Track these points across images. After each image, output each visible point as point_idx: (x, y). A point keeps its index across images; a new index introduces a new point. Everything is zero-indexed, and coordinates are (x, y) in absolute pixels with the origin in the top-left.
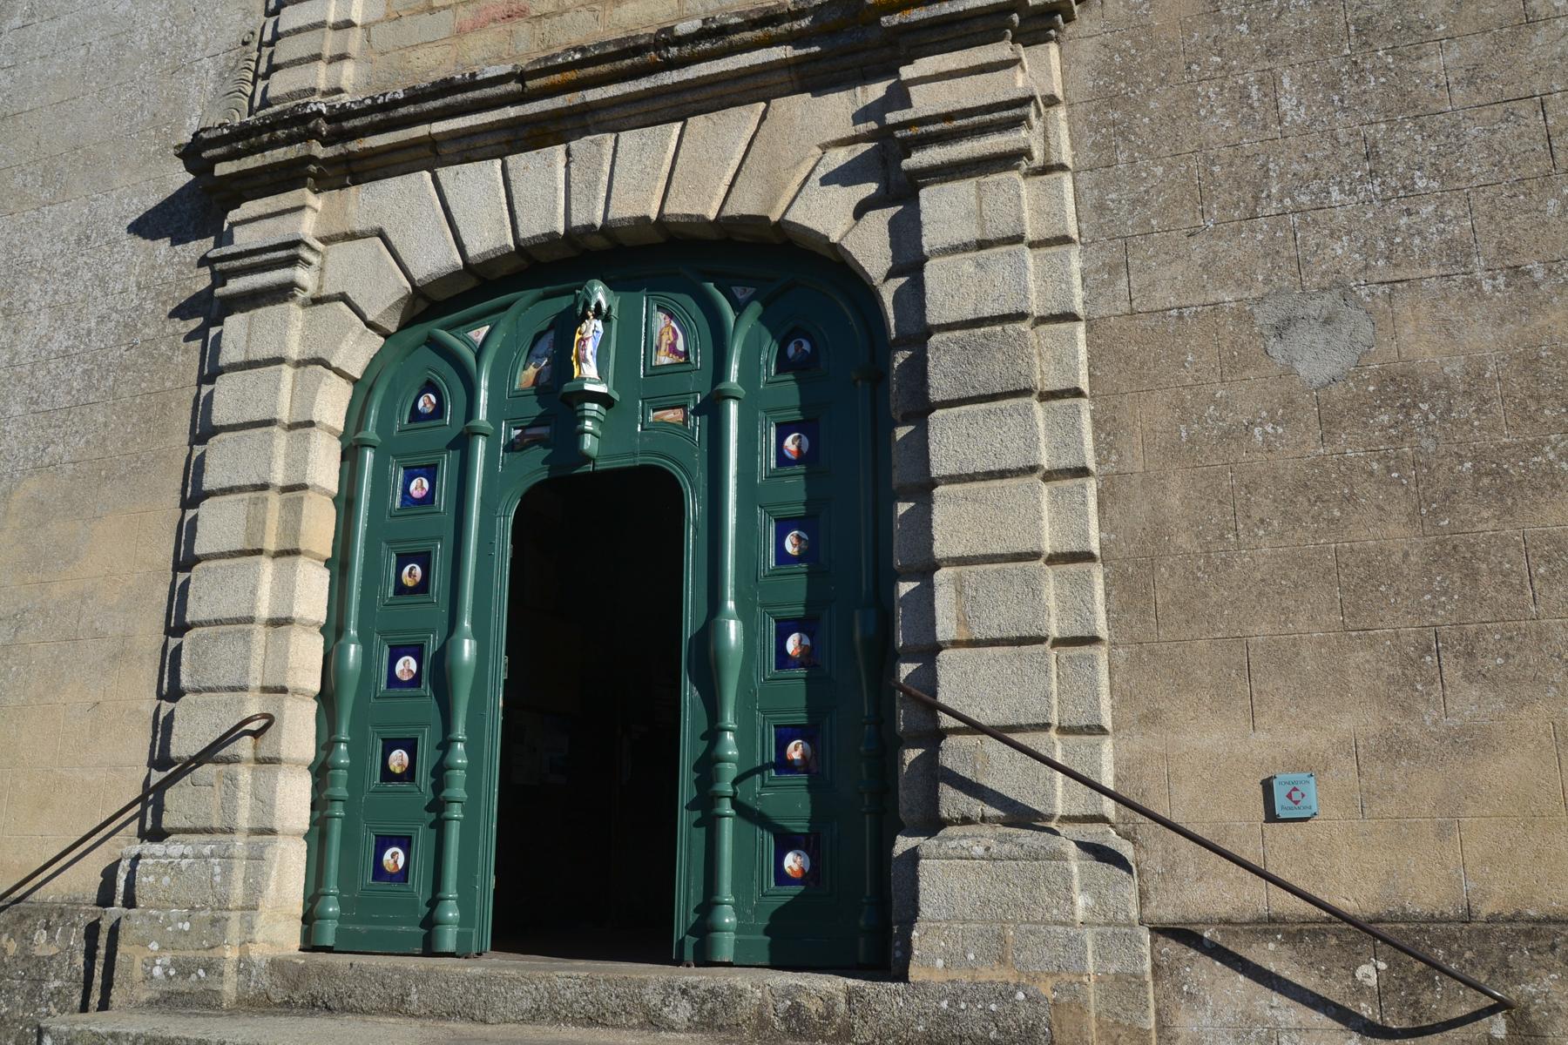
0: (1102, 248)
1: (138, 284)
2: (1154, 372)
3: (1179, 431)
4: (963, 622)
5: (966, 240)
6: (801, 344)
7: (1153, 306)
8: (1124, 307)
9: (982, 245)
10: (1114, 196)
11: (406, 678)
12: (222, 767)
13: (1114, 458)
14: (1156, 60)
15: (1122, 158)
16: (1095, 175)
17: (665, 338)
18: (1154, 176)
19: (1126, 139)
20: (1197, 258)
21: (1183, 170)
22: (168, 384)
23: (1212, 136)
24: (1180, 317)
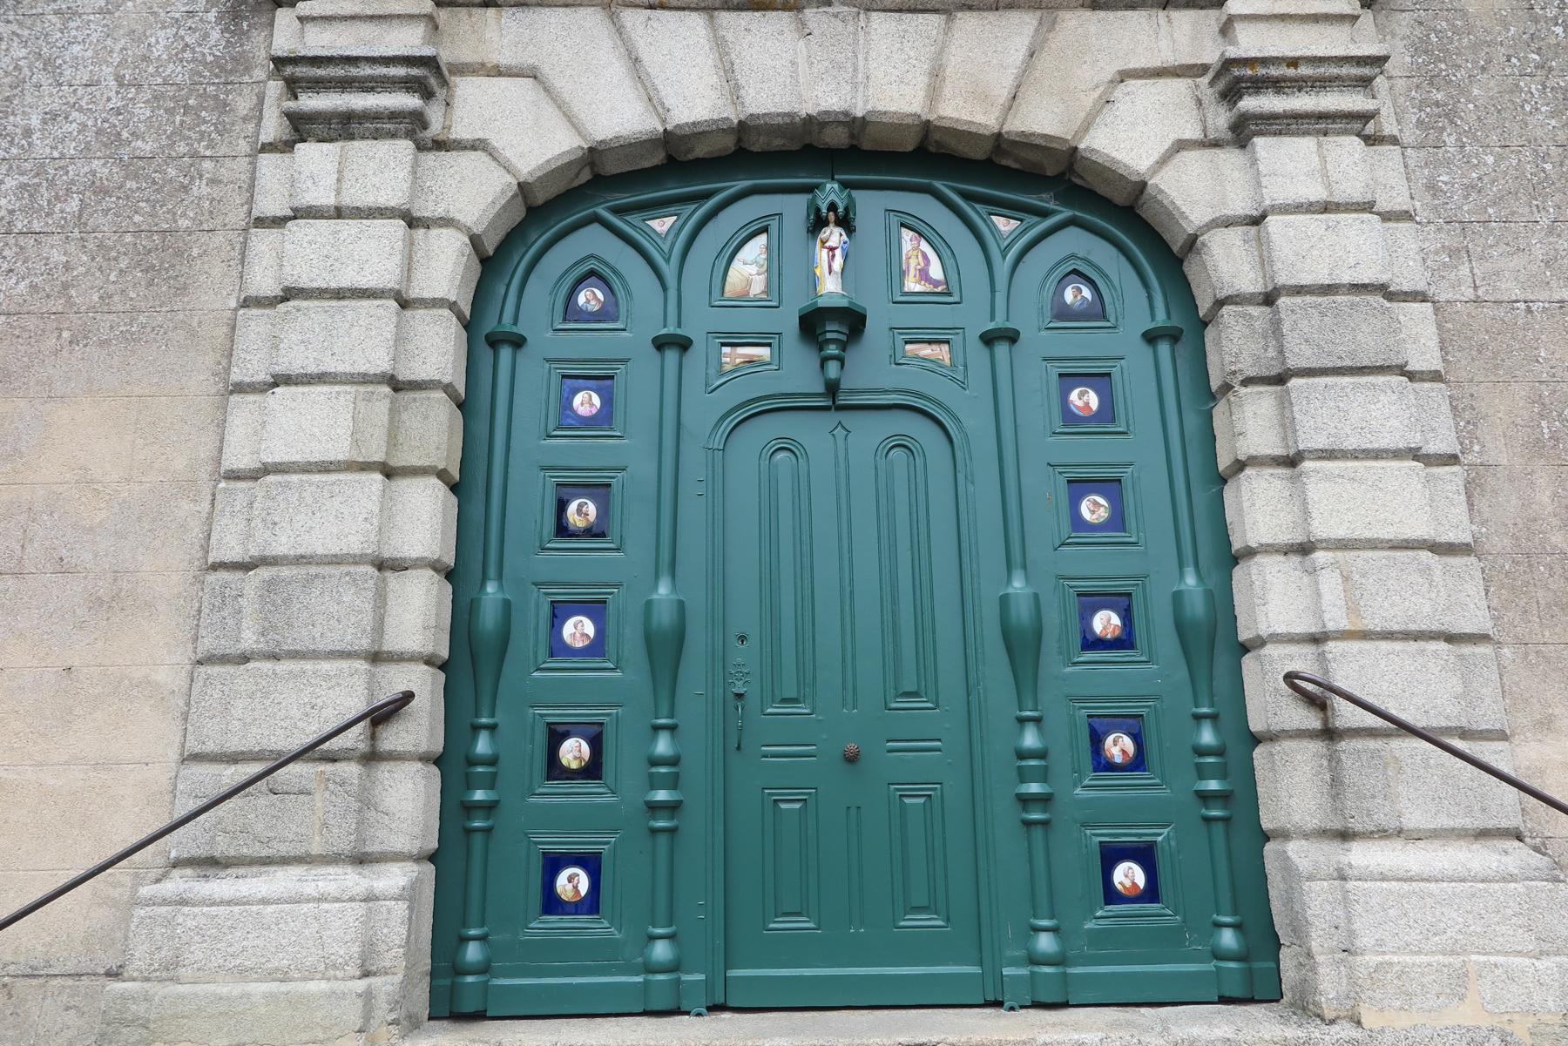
0: (1439, 230)
1: (119, 79)
2: (1508, 363)
3: (1539, 426)
4: (1352, 609)
5: (1313, 199)
6: (1080, 291)
7: (1499, 297)
8: (1469, 293)
9: (1326, 208)
10: (1445, 178)
11: (579, 644)
12: (328, 768)
13: (1476, 448)
14: (1475, 47)
15: (1450, 140)
16: (1423, 153)
17: (913, 262)
18: (1485, 164)
19: (1452, 122)
20: (1539, 252)
21: (1514, 163)
22: (184, 223)
23: (1539, 133)
24: (1529, 310)
